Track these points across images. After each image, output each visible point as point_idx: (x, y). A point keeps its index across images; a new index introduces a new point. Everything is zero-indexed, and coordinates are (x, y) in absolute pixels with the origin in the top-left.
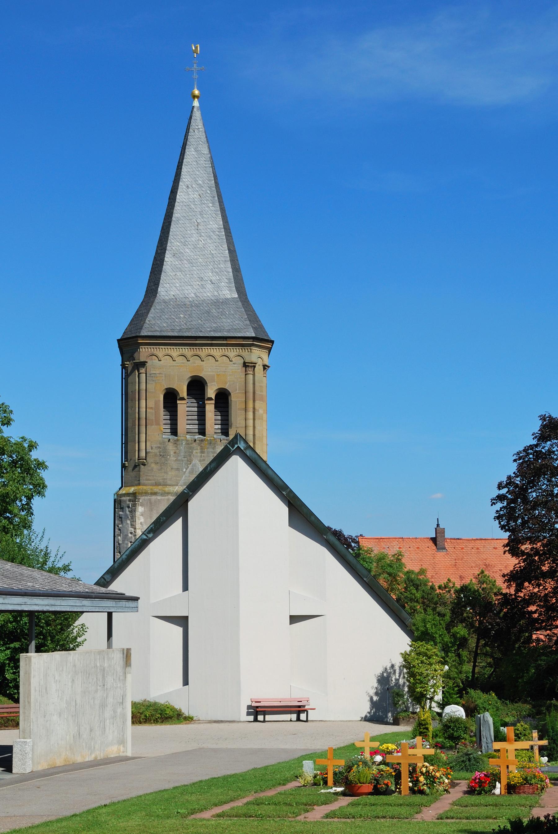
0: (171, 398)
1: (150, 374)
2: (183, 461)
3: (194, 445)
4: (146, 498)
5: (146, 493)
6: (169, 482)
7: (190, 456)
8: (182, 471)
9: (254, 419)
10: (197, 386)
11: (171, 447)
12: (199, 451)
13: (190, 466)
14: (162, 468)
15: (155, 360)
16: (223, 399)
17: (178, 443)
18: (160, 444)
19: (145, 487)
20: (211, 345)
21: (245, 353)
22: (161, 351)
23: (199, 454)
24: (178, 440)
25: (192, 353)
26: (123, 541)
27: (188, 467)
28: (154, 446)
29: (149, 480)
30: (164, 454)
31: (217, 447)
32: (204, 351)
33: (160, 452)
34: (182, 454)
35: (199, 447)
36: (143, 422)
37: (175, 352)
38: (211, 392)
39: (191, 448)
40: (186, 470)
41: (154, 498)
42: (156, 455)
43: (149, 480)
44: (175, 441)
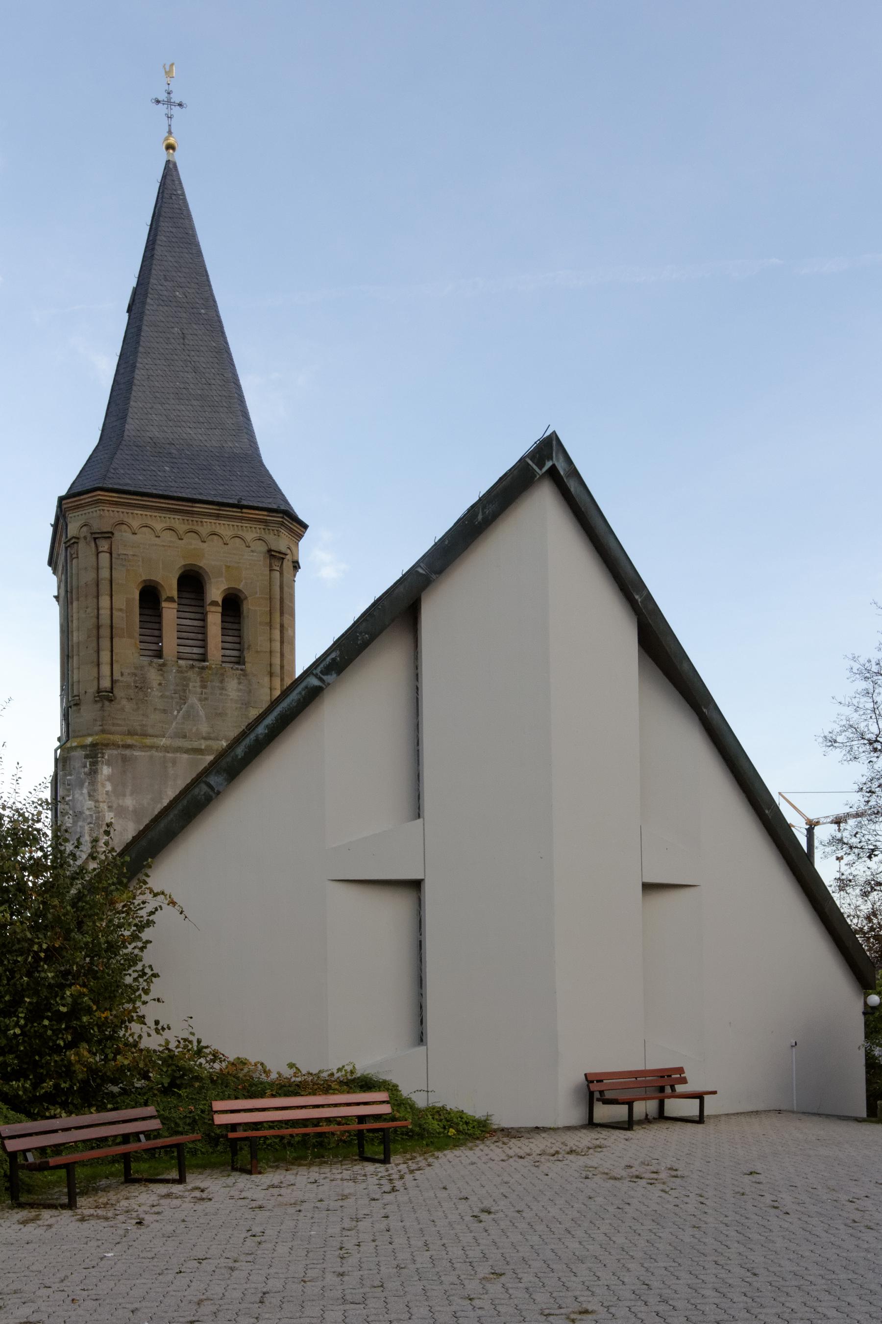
0: (150, 597)
1: (119, 555)
2: (172, 698)
3: (190, 674)
4: (115, 752)
5: (116, 746)
6: (150, 731)
7: (184, 691)
8: (172, 713)
9: (282, 642)
10: (192, 582)
11: (153, 676)
12: (199, 684)
13: (185, 708)
14: (138, 708)
15: (125, 531)
16: (233, 605)
17: (164, 669)
18: (136, 668)
19: (111, 737)
20: (218, 516)
21: (270, 537)
22: (136, 518)
23: (199, 690)
24: (164, 665)
25: (186, 527)
26: (75, 823)
27: (181, 709)
28: (126, 671)
29: (118, 725)
30: (142, 687)
31: (226, 679)
32: (207, 526)
33: (135, 682)
34: (172, 687)
35: (198, 679)
36: (105, 632)
37: (159, 522)
38: (215, 592)
39: (185, 678)
40: (178, 712)
41: (127, 752)
42: (128, 687)
43: (118, 725)
44: (160, 665)
